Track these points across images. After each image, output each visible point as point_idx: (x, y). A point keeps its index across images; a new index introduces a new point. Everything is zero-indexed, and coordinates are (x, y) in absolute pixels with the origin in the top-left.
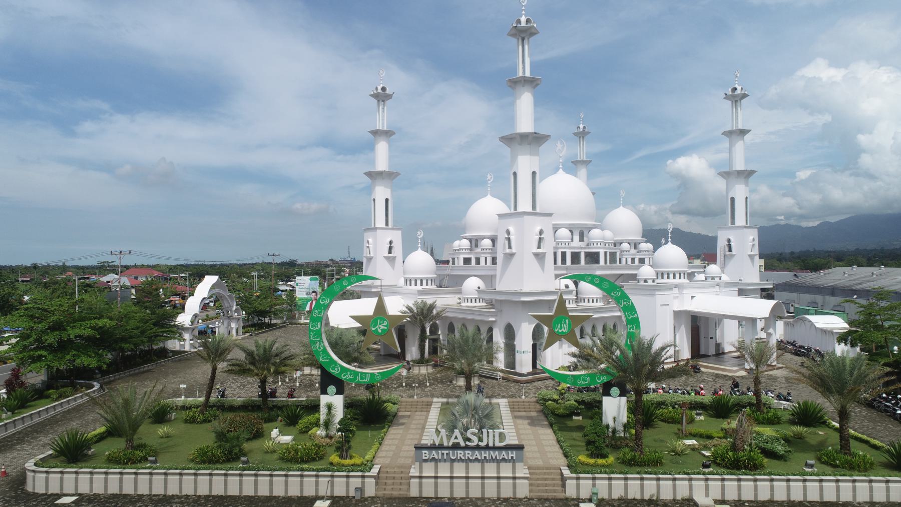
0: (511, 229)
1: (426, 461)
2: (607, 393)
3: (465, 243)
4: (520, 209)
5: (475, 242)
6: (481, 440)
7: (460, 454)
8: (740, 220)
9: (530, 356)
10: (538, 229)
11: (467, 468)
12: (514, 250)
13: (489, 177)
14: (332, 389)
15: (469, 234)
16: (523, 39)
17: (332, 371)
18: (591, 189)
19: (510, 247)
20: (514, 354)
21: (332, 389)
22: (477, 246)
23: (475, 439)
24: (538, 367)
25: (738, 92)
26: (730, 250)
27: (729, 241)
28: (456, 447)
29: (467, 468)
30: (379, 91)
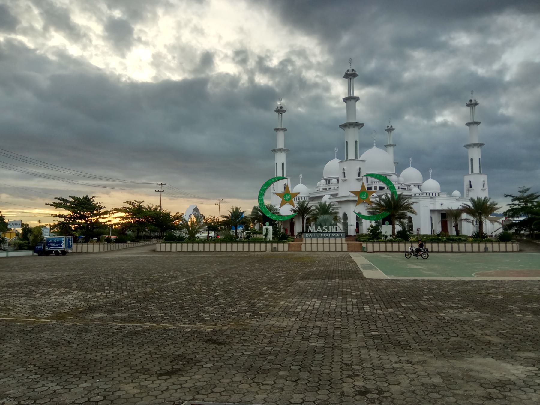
0: (345, 168)
1: (307, 237)
2: (384, 224)
3: (323, 182)
4: (349, 158)
5: (328, 181)
6: (329, 230)
7: (320, 235)
8: (476, 169)
9: (355, 227)
10: (358, 167)
11: (323, 240)
12: (346, 178)
13: (336, 149)
14: (267, 223)
15: (325, 177)
16: (351, 79)
17: (267, 216)
18: (394, 160)
19: (345, 177)
20: (347, 227)
21: (267, 223)
22: (329, 183)
23: (327, 231)
24: (360, 233)
25: (473, 102)
26: (471, 187)
27: (470, 182)
28: (319, 232)
29: (323, 240)
30: (279, 108)
